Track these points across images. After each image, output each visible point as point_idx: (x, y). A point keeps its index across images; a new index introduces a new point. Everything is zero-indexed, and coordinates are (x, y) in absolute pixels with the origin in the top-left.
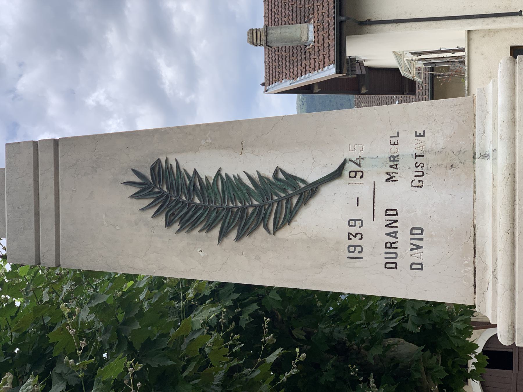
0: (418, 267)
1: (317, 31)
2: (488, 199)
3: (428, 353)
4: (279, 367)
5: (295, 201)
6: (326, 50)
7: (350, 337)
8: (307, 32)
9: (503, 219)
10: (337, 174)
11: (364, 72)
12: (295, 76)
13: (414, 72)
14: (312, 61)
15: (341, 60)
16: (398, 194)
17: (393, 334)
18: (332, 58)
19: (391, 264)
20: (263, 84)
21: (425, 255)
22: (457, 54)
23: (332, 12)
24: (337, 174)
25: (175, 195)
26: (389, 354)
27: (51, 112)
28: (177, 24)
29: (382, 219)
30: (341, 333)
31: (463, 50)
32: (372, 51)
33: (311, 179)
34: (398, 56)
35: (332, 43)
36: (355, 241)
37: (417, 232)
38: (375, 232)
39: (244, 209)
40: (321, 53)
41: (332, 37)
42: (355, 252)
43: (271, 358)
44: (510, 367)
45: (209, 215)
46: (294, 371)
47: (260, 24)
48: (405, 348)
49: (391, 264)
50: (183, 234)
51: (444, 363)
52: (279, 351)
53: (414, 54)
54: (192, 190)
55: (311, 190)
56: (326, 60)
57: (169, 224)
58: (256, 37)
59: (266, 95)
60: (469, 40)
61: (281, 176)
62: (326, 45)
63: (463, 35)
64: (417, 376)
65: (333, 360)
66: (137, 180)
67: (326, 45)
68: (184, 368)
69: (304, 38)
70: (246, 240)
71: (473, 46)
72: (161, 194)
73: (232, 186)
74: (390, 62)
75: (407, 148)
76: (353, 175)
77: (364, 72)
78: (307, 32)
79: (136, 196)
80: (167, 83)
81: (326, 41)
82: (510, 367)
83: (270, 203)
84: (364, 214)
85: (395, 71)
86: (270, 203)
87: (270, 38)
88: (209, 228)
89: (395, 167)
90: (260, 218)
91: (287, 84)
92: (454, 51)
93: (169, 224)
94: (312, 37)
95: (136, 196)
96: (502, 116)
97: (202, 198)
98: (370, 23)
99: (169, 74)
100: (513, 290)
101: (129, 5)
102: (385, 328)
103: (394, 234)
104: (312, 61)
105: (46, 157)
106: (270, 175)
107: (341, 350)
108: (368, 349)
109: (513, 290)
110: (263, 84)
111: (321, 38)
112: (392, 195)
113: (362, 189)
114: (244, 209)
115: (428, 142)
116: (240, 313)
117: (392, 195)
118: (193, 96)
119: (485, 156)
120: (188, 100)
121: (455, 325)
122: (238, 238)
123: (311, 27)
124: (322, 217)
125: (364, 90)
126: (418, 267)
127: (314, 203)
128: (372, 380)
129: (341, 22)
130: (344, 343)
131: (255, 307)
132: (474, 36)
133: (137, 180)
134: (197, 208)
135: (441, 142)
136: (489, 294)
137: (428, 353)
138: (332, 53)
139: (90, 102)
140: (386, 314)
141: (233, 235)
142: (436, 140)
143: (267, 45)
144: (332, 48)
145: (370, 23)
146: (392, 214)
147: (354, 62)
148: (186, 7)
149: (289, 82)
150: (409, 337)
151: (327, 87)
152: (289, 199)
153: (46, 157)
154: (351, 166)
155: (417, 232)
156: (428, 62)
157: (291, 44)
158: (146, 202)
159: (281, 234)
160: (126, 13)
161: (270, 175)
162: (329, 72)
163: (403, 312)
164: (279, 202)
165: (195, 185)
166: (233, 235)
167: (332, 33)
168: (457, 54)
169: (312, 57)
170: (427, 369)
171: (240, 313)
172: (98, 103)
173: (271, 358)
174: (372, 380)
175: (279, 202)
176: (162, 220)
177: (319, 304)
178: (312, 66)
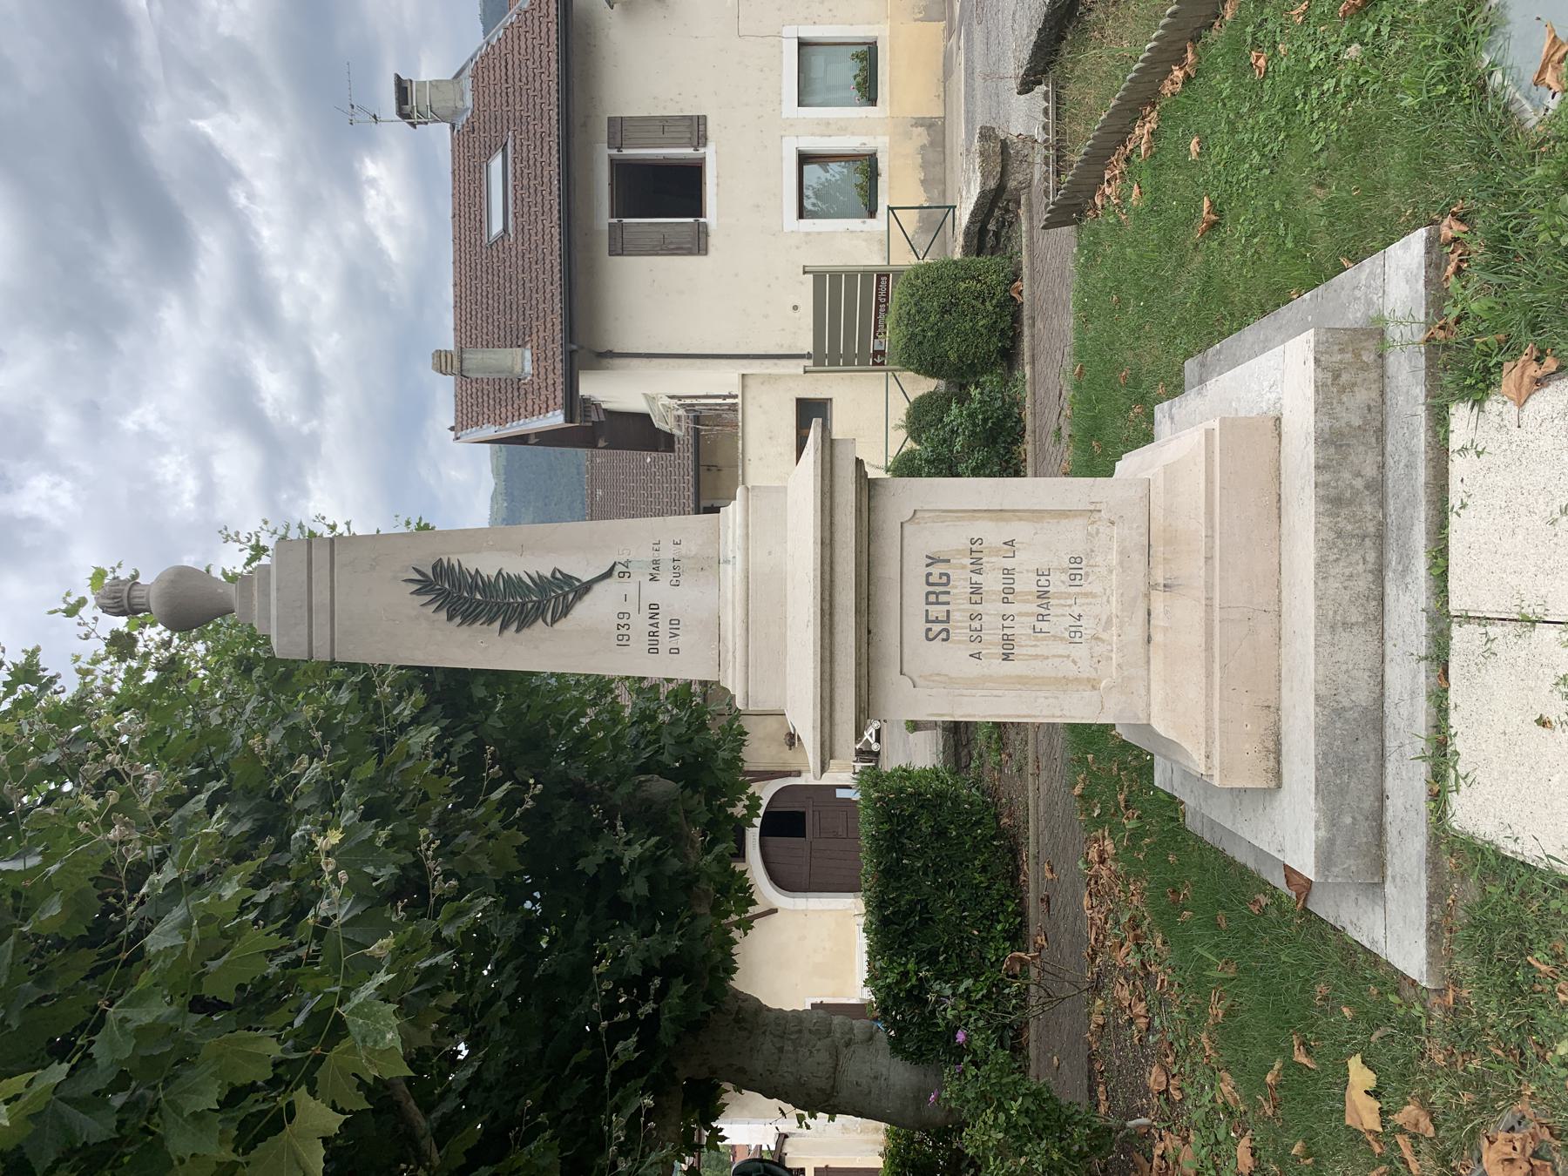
0: (675, 651)
1: (536, 360)
2: (730, 595)
3: (688, 792)
4: (511, 801)
5: (571, 597)
6: (551, 388)
7: (591, 777)
8: (522, 361)
9: (740, 612)
10: (608, 574)
11: (603, 418)
12: (503, 421)
13: (671, 421)
14: (529, 402)
15: (573, 403)
16: (659, 592)
17: (644, 769)
18: (559, 400)
19: (653, 650)
20: (452, 429)
21: (680, 642)
22: (729, 401)
23: (558, 337)
24: (608, 574)
25: (455, 592)
26: (639, 794)
27: (53, 438)
28: (288, 305)
29: (646, 613)
30: (579, 771)
31: (736, 397)
32: (612, 390)
33: (585, 579)
34: (650, 399)
35: (560, 380)
36: (623, 631)
37: (675, 623)
38: (640, 623)
39: (524, 604)
40: (543, 392)
41: (559, 372)
42: (623, 640)
43: (497, 795)
44: (801, 833)
45: (490, 610)
46: (529, 804)
47: (448, 342)
48: (660, 786)
49: (653, 650)
50: (464, 627)
51: (708, 803)
52: (507, 785)
53: (671, 397)
54: (473, 587)
55: (587, 587)
56: (551, 402)
57: (450, 618)
58: (442, 362)
59: (458, 445)
60: (744, 387)
61: (558, 575)
62: (550, 382)
63: (736, 379)
64: (675, 819)
65: (567, 806)
66: (418, 577)
67: (550, 382)
68: (398, 801)
69: (517, 369)
70: (525, 631)
71: (749, 396)
72: (443, 590)
73: (513, 584)
74: (637, 404)
75: (667, 554)
76: (622, 575)
77: (603, 418)
78: (522, 361)
79: (417, 592)
80: (269, 399)
81: (551, 376)
82: (801, 833)
83: (551, 598)
84: (631, 608)
85: (645, 417)
86: (551, 598)
87: (466, 365)
88: (490, 621)
89: (657, 569)
90: (539, 612)
91: (490, 431)
92: (725, 397)
93: (450, 618)
94: (528, 368)
95: (417, 592)
96: (739, 532)
97: (484, 593)
98: (612, 355)
99: (273, 386)
100: (747, 666)
101: (203, 267)
102: (636, 758)
103: (656, 625)
104: (529, 402)
105: (320, 555)
106: (549, 575)
107: (580, 794)
108: (613, 789)
109: (747, 666)
110: (452, 429)
111: (542, 371)
112: (653, 592)
113: (630, 587)
114: (524, 604)
115: (683, 549)
116: (451, 745)
117: (653, 592)
118: (315, 423)
119: (727, 562)
120: (305, 429)
121: (721, 754)
122: (518, 631)
123: (528, 354)
124: (595, 610)
125: (601, 443)
126: (675, 651)
127: (588, 598)
128: (619, 823)
129: (572, 352)
130: (583, 785)
131: (470, 736)
132: (749, 382)
133: (418, 577)
134: (479, 603)
135: (694, 550)
136: (730, 671)
137: (688, 792)
138: (559, 394)
139: (129, 424)
140: (636, 746)
141: (514, 627)
142: (690, 547)
143: (462, 373)
144: (559, 387)
145: (612, 355)
146: (654, 607)
147: (588, 404)
148: (303, 277)
149: (493, 429)
150: (666, 772)
151: (548, 438)
152: (565, 596)
153: (320, 555)
154: (619, 568)
155: (675, 623)
156: (689, 408)
157: (496, 376)
158: (428, 598)
159: (557, 626)
160: (198, 278)
161: (549, 575)
162: (555, 419)
163: (657, 741)
164: (557, 598)
165: (476, 582)
166: (514, 627)
167: (559, 366)
168: (729, 401)
169: (530, 396)
170: (686, 811)
171: (451, 745)
172: (142, 425)
173: (497, 795)
174: (619, 823)
175: (557, 598)
176: (443, 615)
177: (552, 732)
178: (529, 408)
